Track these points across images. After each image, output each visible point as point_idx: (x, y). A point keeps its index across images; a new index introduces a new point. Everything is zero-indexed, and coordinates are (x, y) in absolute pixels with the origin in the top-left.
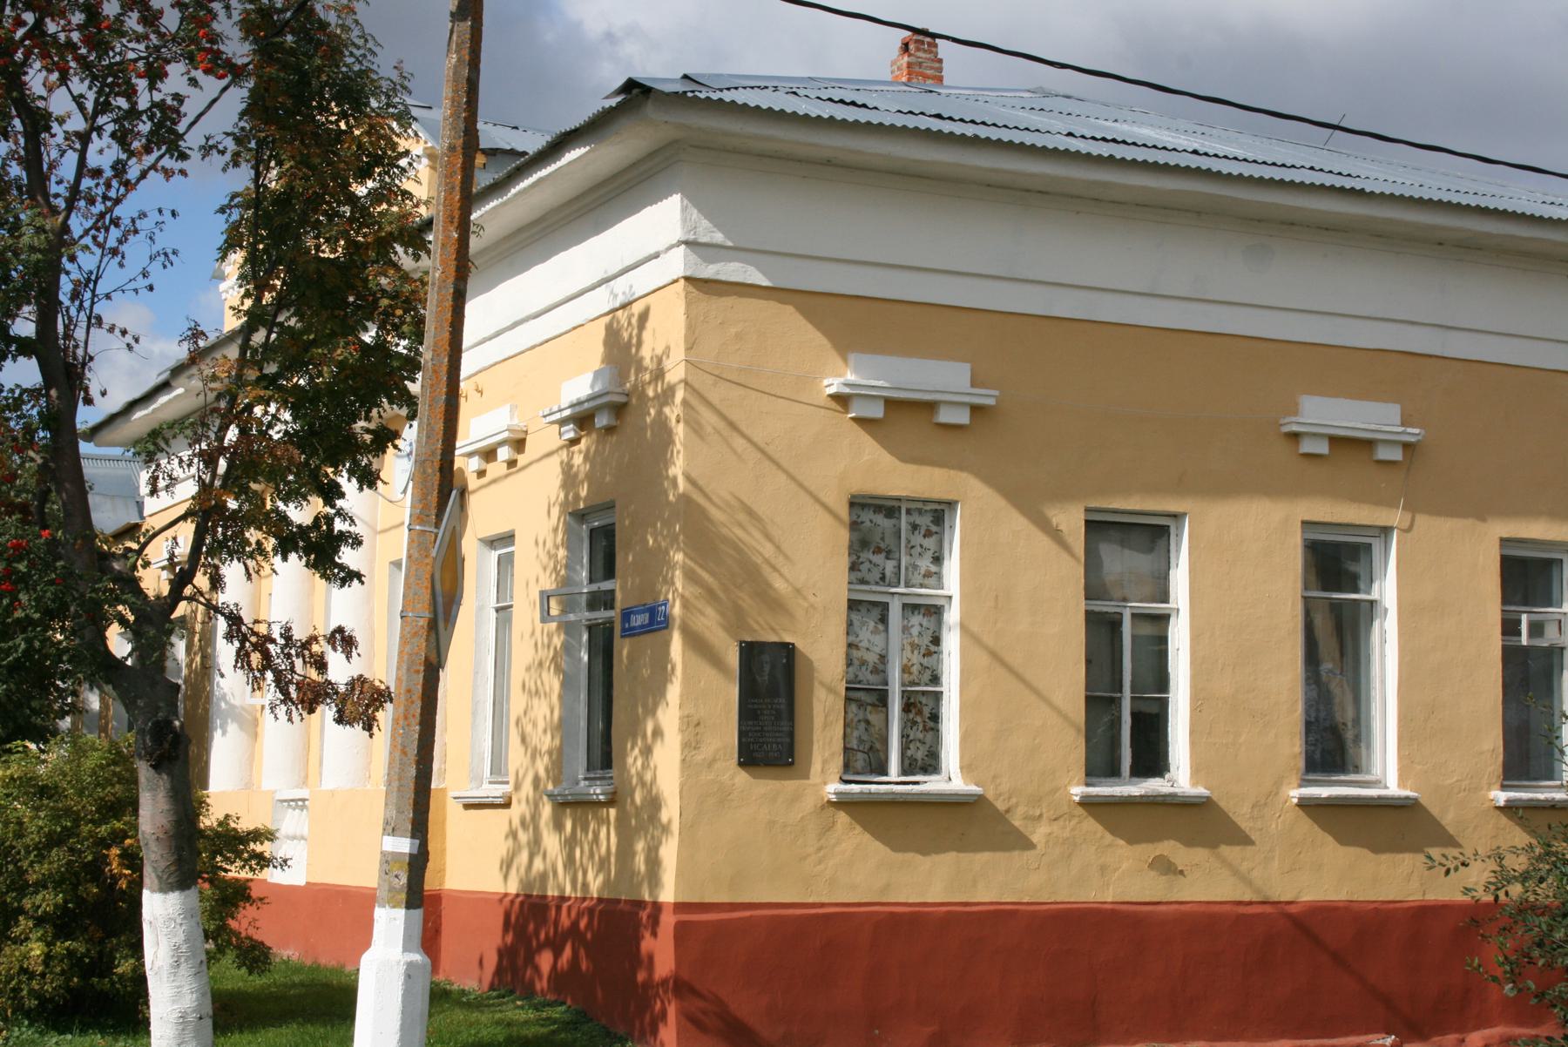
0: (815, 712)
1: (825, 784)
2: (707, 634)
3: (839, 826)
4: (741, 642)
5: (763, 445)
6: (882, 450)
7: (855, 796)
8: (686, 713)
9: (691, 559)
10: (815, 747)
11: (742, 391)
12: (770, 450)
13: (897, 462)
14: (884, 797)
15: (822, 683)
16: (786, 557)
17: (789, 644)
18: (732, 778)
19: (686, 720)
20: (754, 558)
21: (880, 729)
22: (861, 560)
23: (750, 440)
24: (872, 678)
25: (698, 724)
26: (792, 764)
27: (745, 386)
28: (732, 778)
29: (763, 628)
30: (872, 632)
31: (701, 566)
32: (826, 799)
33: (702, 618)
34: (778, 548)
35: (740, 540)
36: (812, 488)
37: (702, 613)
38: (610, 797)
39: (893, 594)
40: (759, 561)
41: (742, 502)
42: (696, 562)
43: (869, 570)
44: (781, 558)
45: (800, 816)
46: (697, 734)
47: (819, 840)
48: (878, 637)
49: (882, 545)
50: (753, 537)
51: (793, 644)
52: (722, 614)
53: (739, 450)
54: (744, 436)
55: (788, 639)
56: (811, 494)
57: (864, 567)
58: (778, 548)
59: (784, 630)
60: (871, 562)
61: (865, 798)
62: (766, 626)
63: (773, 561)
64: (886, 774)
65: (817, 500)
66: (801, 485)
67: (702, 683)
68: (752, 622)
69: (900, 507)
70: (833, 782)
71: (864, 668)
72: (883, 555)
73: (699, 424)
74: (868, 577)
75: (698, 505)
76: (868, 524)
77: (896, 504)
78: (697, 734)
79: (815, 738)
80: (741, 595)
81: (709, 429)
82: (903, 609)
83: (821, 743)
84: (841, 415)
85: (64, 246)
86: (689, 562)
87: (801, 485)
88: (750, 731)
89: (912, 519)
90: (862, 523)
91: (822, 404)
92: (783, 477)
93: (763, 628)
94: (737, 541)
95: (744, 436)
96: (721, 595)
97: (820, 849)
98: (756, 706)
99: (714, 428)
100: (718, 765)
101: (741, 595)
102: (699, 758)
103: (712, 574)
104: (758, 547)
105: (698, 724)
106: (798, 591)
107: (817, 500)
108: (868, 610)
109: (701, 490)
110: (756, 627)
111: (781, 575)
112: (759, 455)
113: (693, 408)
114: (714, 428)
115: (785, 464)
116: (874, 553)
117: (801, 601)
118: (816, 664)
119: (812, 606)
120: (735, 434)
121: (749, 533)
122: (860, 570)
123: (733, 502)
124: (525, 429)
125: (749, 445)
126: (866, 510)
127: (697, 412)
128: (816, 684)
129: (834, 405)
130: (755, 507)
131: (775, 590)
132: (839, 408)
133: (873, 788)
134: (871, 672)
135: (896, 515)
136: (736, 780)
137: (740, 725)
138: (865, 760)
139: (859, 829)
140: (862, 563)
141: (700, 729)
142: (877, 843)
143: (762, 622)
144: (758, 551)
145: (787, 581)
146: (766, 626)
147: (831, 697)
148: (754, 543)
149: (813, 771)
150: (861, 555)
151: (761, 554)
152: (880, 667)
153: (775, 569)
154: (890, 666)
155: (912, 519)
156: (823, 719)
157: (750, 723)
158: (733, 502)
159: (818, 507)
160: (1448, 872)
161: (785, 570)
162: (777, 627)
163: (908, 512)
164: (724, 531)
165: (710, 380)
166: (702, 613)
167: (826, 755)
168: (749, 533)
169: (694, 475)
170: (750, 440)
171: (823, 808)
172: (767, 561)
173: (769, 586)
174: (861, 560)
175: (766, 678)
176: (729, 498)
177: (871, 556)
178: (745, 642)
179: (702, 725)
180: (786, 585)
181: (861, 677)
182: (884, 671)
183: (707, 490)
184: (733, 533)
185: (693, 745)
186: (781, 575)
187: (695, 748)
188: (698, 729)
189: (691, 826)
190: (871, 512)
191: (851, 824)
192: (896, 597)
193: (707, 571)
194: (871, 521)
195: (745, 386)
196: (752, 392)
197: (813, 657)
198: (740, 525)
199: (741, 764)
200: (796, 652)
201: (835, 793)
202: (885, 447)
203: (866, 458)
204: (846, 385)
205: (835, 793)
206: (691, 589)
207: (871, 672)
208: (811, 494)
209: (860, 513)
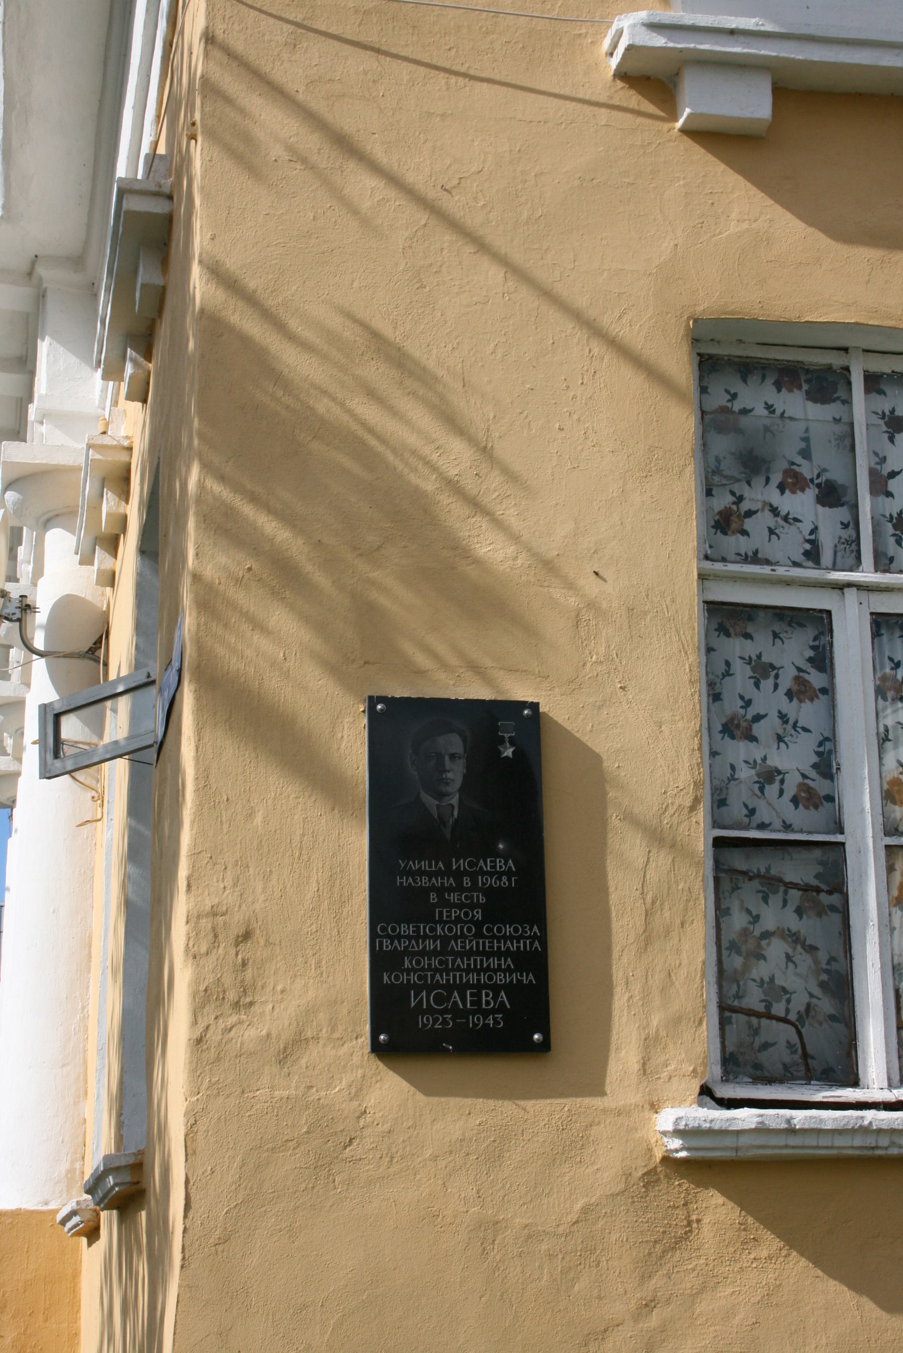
0: (614, 898)
1: (655, 1108)
2: (273, 683)
3: (707, 1234)
4: (372, 701)
5: (432, 193)
6: (779, 210)
7: (744, 1141)
8: (208, 904)
9: (222, 478)
10: (619, 1000)
11: (369, 61)
12: (454, 205)
13: (824, 240)
14: (839, 1141)
15: (629, 818)
16: (511, 476)
17: (523, 705)
18: (357, 1092)
19: (206, 924)
20: (413, 478)
21: (832, 959)
22: (745, 506)
23: (393, 180)
24: (799, 816)
25: (247, 936)
26: (545, 1046)
27: (378, 51)
28: (357, 1092)
29: (444, 665)
30: (790, 694)
31: (254, 499)
32: (658, 1155)
33: (257, 638)
34: (486, 451)
35: (371, 431)
36: (581, 301)
37: (259, 626)
38: (127, 1178)
39: (841, 587)
40: (429, 485)
41: (375, 335)
42: (237, 488)
43: (771, 532)
44: (495, 479)
45: (578, 1206)
46: (244, 964)
47: (645, 1278)
48: (807, 706)
49: (807, 470)
50: (408, 422)
51: (535, 706)
52: (320, 627)
53: (366, 205)
54: (375, 168)
55: (520, 692)
56: (576, 316)
57: (758, 525)
58: (486, 451)
59: (511, 670)
60: (775, 511)
61: (776, 1147)
62: (454, 661)
63: (470, 485)
64: (855, 1082)
65: (595, 330)
66: (548, 295)
67: (258, 819)
68: (409, 648)
69: (847, 369)
70: (678, 1102)
71: (772, 790)
72: (811, 494)
73: (247, 138)
74: (768, 549)
75: (245, 341)
76: (761, 411)
77: (835, 360)
78: (244, 964)
79: (618, 975)
80: (376, 575)
81: (277, 151)
82: (876, 634)
83: (636, 988)
84: (659, 124)
85: (508, 877)
86: (216, 488)
87: (548, 295)
88: (406, 952)
89: (884, 404)
90: (745, 412)
91: (603, 98)
92: (494, 274)
93: (444, 665)
94: (361, 432)
95: (375, 168)
96: (322, 579)
97: (649, 1305)
98: (424, 881)
99: (290, 149)
100: (313, 1054)
101: (376, 575)
102: (250, 1035)
103: (288, 519)
104: (427, 450)
105: (247, 936)
106: (549, 566)
107: (595, 330)
108: (776, 635)
109: (250, 299)
110: (422, 660)
111: (498, 524)
112: (423, 217)
113: (229, 101)
114: (290, 149)
115: (498, 241)
116: (782, 488)
117: (558, 593)
118: (609, 764)
119: (592, 605)
120: (351, 165)
121: (395, 413)
122: (745, 533)
123: (350, 333)
124: (126, 443)
125: (392, 193)
126: (754, 379)
127: (242, 111)
128: (614, 821)
129: (633, 99)
130: (414, 349)
131: (477, 562)
132: (651, 108)
133: (800, 1117)
134: (795, 801)
135: (841, 393)
136: (371, 1100)
137: (373, 935)
138: (790, 1046)
139: (770, 1243)
140: (750, 514)
141: (252, 951)
142: (833, 1285)
143: (442, 649)
144: (427, 463)
145: (515, 538)
146: (454, 661)
147: (662, 860)
148: (412, 440)
149: (614, 1069)
150: (747, 492)
151: (434, 468)
152: (820, 786)
153: (476, 505)
154: (845, 779)
155: (884, 404)
156: (640, 921)
157: (407, 929)
158: (350, 333)
159: (597, 348)
160: (600, 1298)
161: (509, 513)
162: (488, 662)
163: (873, 382)
164: (322, 406)
165: (280, 33)
166: (259, 626)
167: (656, 1020)
168: (395, 413)
169: (232, 263)
170: (393, 180)
171: (650, 1179)
172: (453, 486)
173: (462, 551)
174: (745, 506)
175: (455, 801)
176: (336, 322)
177: (775, 497)
178: (382, 699)
179: (259, 936)
180: (511, 550)
181: (763, 813)
182: (830, 799)
183: (271, 302)
184: (350, 412)
185: (232, 995)
186: (498, 524)
187: (236, 1005)
188: (246, 950)
189: (224, 1240)
190: (770, 381)
191: (743, 1225)
192: (851, 595)
193: (270, 510)
194: (769, 408)
195: (378, 51)
196: (396, 64)
197: (600, 744)
198: (372, 394)
199: (377, 1049)
200: (549, 742)
201: (678, 1133)
202: (788, 207)
203: (734, 228)
204: (654, 27)
205: (678, 1133)
206: (223, 559)
207: (795, 801)
208: (576, 316)
209: (737, 386)
